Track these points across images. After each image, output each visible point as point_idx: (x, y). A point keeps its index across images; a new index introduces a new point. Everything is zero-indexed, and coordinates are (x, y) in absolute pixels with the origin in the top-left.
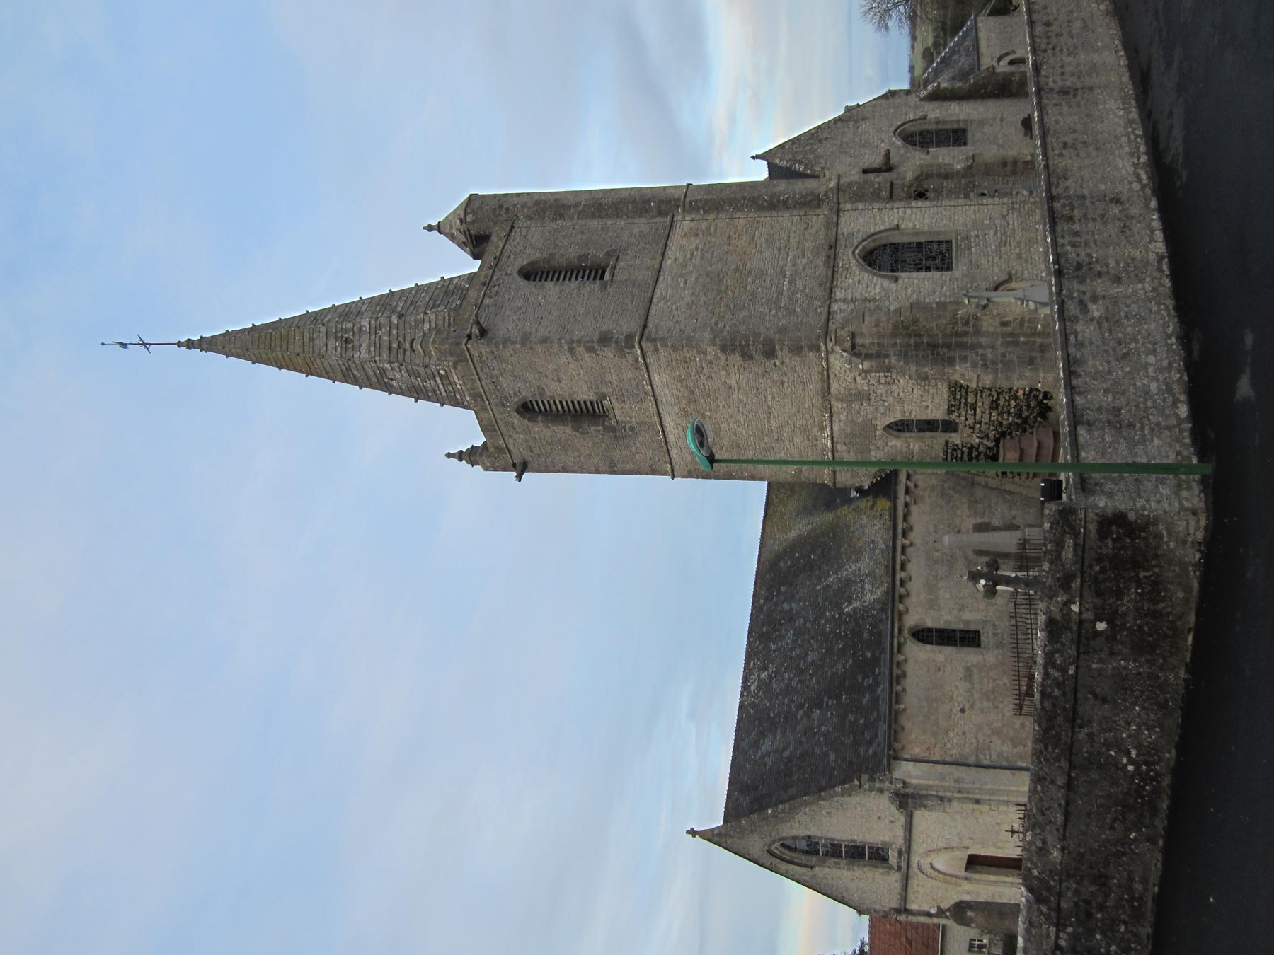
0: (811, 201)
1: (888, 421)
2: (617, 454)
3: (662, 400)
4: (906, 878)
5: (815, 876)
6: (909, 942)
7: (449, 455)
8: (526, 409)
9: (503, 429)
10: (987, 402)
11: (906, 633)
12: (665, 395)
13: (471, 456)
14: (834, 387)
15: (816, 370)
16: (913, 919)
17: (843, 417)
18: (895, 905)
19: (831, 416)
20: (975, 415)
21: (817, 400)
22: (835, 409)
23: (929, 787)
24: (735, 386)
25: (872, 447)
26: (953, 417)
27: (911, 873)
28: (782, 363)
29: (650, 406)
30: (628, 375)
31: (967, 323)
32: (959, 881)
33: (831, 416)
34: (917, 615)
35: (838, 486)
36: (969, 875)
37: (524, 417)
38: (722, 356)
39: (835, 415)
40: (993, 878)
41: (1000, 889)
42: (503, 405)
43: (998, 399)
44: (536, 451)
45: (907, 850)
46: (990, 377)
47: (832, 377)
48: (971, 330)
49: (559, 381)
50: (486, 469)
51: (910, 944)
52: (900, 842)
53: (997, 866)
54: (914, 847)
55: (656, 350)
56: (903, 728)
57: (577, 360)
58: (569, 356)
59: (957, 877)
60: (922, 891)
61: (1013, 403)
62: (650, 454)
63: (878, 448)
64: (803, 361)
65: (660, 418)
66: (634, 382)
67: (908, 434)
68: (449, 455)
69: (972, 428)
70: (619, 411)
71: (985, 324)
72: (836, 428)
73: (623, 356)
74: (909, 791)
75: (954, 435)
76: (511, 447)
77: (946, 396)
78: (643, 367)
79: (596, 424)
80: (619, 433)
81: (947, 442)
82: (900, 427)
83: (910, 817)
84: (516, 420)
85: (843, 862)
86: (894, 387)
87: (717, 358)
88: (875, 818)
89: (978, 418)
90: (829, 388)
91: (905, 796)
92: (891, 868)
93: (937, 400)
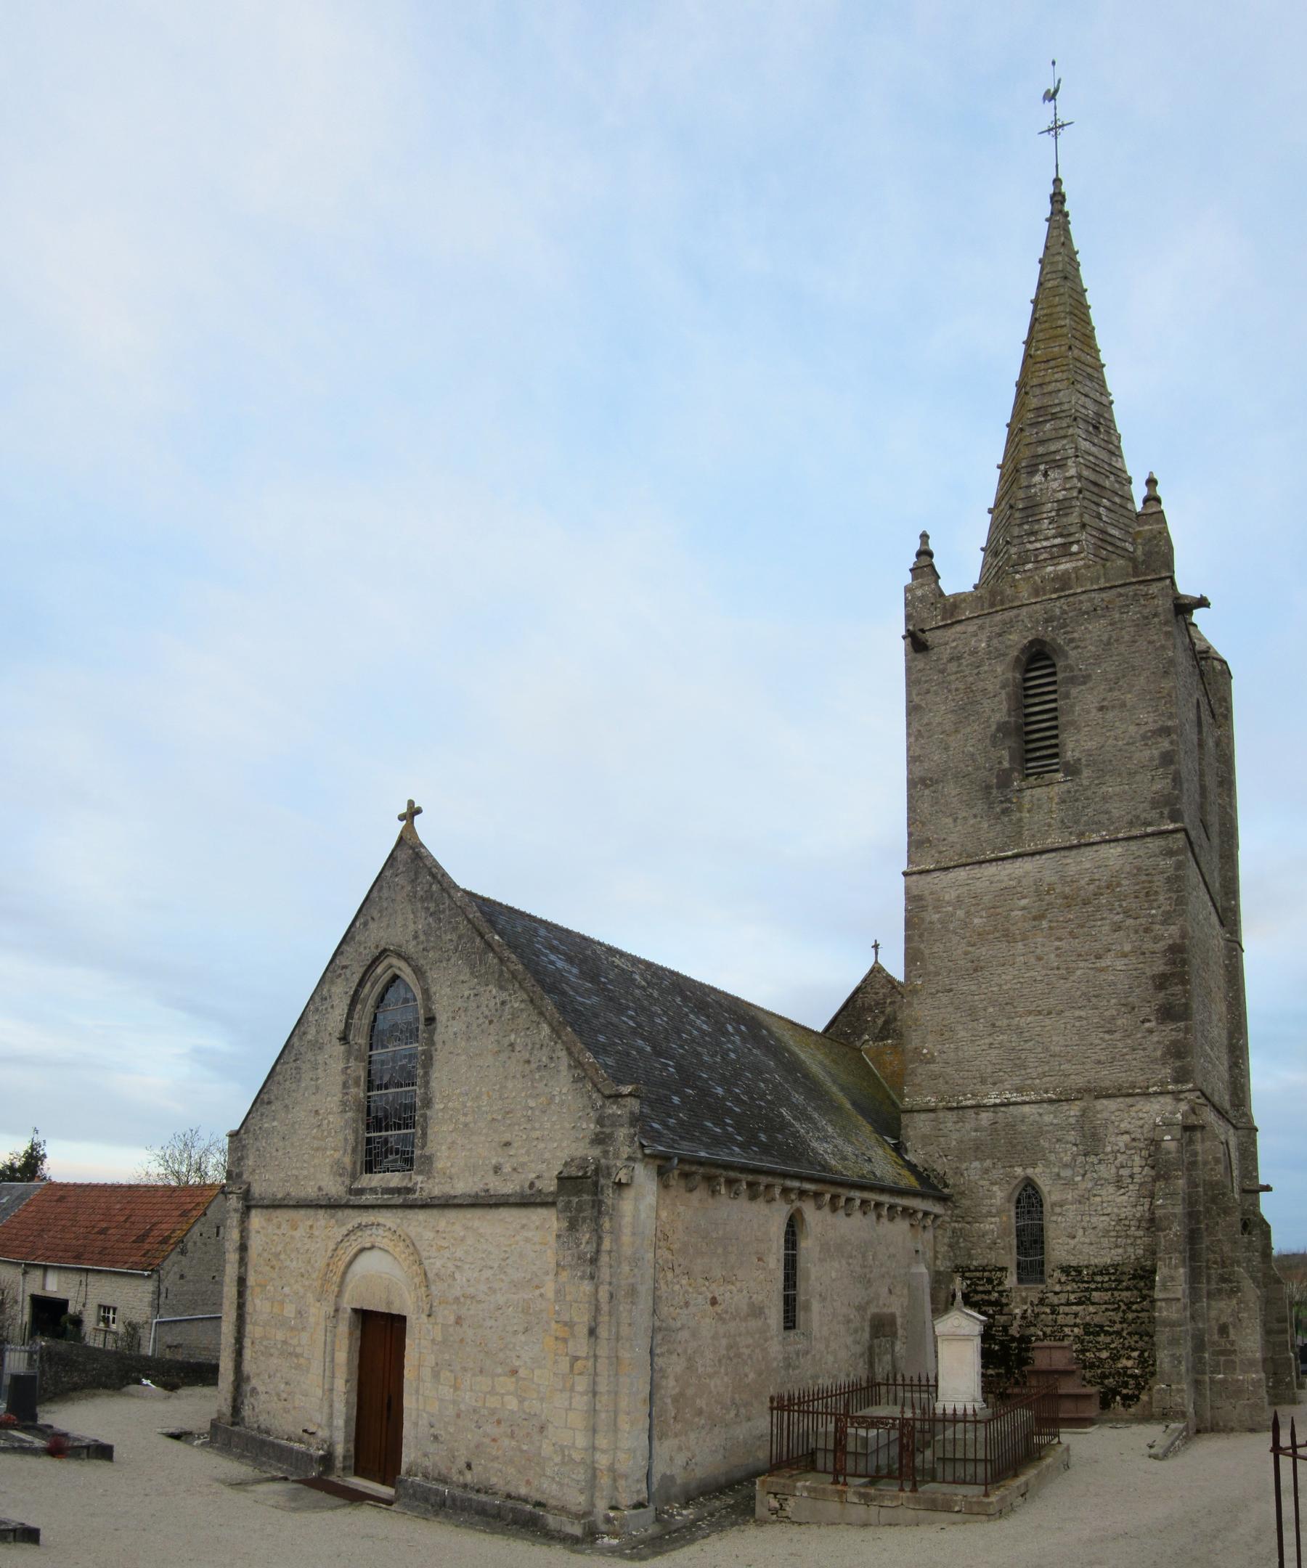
0: (1237, 1095)
1: (1044, 1184)
2: (951, 790)
3: (1071, 859)
4: (332, 1206)
5: (317, 1046)
6: (103, 1231)
7: (924, 537)
8: (1038, 657)
9: (998, 617)
10: (1097, 1319)
11: (797, 1204)
12: (1086, 859)
13: (924, 565)
14: (1108, 1107)
15: (1140, 1079)
16: (234, 1220)
17: (1048, 1119)
18: (257, 1190)
19: (1051, 1101)
20: (1068, 1304)
21: (1080, 1081)
22: (1065, 1106)
23: (616, 1233)
24: (1106, 962)
25: (988, 1163)
26: (1057, 1274)
27: (340, 1214)
28: (1150, 1031)
29: (1054, 839)
30: (1117, 809)
31: (1223, 1279)
32: (332, 1297)
33: (1051, 1101)
34: (814, 1217)
35: (905, 1119)
36: (346, 1315)
37: (1023, 651)
38: (1161, 946)
39: (1052, 1108)
40: (342, 1356)
41: (316, 1367)
42: (1047, 621)
43: (1107, 1333)
44: (953, 667)
45: (407, 1202)
46: (1175, 1316)
47: (1129, 1100)
48: (1213, 1286)
49: (1101, 709)
50: (908, 589)
51: (100, 1233)
52: (435, 1188)
53: (786, 1311)
54: (421, 1215)
55: (1170, 853)
56: (691, 1190)
57: (1144, 737)
58: (1151, 727)
59: (339, 1295)
60: (297, 1234)
61: (1104, 1355)
62: (953, 838)
63: (986, 1171)
64: (1154, 1061)
65: (1033, 854)
66: (1104, 817)
67: (1013, 1213)
68: (924, 537)
69: (1042, 1302)
70: (1043, 800)
71: (1222, 1304)
72: (1026, 1109)
73: (1155, 804)
74: (609, 1195)
75: (1015, 1278)
76: (958, 628)
77: (1094, 1261)
78: (1136, 832)
79: (1012, 759)
80: (997, 793)
81: (1003, 1269)
82: (1029, 1200)
83: (528, 1201)
84: (1017, 640)
85: (359, 1092)
86: (1111, 1189)
87: (1156, 939)
88: (507, 1137)
89: (1062, 1309)
90: (1108, 1096)
91: (596, 1190)
92: (354, 1177)
93: (1086, 1249)
